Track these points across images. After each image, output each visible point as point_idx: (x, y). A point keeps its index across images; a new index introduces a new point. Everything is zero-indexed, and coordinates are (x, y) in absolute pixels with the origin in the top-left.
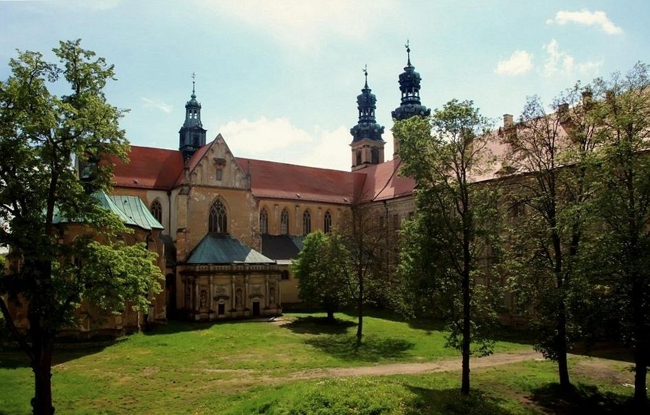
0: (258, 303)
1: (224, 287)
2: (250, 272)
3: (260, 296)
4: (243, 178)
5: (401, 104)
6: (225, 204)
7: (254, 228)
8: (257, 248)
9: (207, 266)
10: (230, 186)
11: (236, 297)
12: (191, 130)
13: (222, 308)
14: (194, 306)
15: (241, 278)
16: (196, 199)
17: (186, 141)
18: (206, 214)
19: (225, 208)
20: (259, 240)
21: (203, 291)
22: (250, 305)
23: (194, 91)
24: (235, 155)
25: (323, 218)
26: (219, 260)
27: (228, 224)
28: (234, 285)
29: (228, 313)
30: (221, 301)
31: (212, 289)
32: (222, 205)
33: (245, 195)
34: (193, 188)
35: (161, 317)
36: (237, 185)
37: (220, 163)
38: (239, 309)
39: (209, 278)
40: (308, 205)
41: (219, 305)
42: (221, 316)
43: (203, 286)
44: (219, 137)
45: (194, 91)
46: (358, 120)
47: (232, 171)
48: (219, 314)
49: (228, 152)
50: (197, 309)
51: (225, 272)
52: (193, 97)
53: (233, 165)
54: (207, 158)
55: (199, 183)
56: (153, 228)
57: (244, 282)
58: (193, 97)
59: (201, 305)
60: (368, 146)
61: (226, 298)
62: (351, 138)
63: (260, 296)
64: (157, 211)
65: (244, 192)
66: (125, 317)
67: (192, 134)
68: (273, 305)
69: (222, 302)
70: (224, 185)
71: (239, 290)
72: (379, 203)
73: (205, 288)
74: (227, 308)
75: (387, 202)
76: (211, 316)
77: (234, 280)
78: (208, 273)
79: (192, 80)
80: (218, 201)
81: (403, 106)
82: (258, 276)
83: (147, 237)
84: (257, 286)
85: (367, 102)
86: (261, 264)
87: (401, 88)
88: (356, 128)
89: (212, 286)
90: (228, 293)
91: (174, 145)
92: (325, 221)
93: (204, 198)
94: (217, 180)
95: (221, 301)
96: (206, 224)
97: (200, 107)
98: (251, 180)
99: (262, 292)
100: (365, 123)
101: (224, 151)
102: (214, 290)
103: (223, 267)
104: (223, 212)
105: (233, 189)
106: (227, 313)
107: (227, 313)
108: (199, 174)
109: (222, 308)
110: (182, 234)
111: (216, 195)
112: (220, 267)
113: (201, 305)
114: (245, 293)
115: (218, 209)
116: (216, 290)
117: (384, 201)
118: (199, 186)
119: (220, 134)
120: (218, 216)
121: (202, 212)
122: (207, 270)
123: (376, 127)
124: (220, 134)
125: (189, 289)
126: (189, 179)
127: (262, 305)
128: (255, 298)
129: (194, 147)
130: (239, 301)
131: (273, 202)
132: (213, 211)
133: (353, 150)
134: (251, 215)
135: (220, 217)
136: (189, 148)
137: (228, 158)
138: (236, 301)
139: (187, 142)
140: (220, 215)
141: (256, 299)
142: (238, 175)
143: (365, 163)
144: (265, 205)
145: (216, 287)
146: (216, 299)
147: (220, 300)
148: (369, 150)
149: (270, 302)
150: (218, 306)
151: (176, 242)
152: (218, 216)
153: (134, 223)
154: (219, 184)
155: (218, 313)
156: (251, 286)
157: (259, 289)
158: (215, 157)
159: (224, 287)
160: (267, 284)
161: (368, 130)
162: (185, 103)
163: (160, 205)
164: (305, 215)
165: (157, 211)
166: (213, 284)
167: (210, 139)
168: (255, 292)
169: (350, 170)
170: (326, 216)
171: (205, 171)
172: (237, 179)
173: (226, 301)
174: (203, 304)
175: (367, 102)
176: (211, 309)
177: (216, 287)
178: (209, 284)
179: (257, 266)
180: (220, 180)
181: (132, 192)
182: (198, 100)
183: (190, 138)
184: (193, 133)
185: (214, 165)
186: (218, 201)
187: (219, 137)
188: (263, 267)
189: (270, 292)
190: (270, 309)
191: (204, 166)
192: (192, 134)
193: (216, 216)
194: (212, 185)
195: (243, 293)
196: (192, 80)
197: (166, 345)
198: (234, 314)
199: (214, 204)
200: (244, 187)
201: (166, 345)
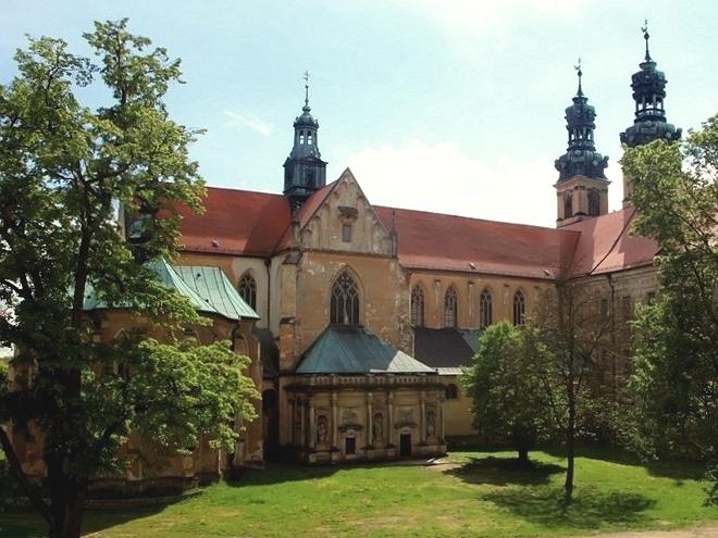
0: (354, 439)
1: (354, 411)
2: (396, 387)
3: (412, 425)
4: (384, 238)
5: (635, 121)
6: (356, 280)
7: (403, 317)
8: (407, 348)
9: (327, 378)
10: (364, 251)
11: (374, 427)
12: (303, 161)
13: (351, 443)
14: (307, 442)
15: (381, 396)
16: (310, 271)
17: (294, 179)
18: (326, 296)
19: (356, 285)
20: (410, 337)
21: (321, 417)
22: (395, 439)
23: (307, 101)
24: (376, 197)
25: (512, 301)
26: (346, 367)
27: (361, 310)
28: (370, 407)
29: (362, 452)
30: (350, 433)
31: (335, 414)
32: (351, 281)
33: (388, 266)
34: (306, 254)
35: (256, 458)
36: (376, 249)
37: (349, 214)
38: (378, 445)
39: (331, 397)
40: (488, 281)
41: (347, 439)
42: (349, 457)
43: (321, 408)
44: (347, 173)
45: (307, 101)
46: (567, 146)
47: (368, 227)
48: (347, 453)
49: (362, 197)
50: (312, 445)
51: (356, 387)
52: (306, 110)
53: (369, 218)
54: (327, 206)
55: (315, 246)
56: (242, 317)
57: (387, 403)
58: (306, 110)
59: (318, 439)
60: (583, 188)
61: (358, 428)
62: (556, 175)
63: (412, 425)
64: (248, 290)
65: (386, 260)
66: (198, 458)
67: (304, 168)
68: (432, 440)
69: (351, 434)
70: (355, 250)
71: (378, 416)
72: (600, 278)
73: (323, 413)
74: (360, 443)
75: (613, 276)
76: (335, 457)
77: (371, 399)
78: (330, 388)
79: (305, 83)
80: (345, 274)
81: (639, 124)
82: (408, 393)
83: (233, 332)
84: (407, 409)
85: (580, 118)
86: (413, 374)
87: (634, 96)
88: (563, 158)
89: (335, 408)
90: (360, 421)
91: (276, 186)
92: (515, 306)
93: (323, 270)
94: (343, 241)
95: (350, 433)
96: (327, 311)
97: (317, 126)
98: (397, 241)
99: (415, 418)
100: (578, 152)
101: (355, 196)
102: (339, 416)
103: (353, 378)
104: (353, 292)
105: (369, 255)
106: (359, 451)
107: (359, 451)
108: (315, 232)
109: (351, 443)
110: (288, 326)
111: (342, 264)
112: (348, 378)
113: (318, 439)
114: (389, 420)
115: (345, 287)
116: (341, 415)
117: (609, 275)
118: (316, 251)
119: (348, 169)
120: (345, 298)
121: (320, 293)
122: (328, 383)
123: (595, 157)
124: (348, 169)
125: (300, 414)
126: (299, 240)
127: (415, 439)
128: (404, 429)
129: (307, 189)
130: (379, 432)
131: (432, 277)
132: (337, 291)
133: (559, 194)
134: (398, 296)
135: (349, 300)
136: (299, 190)
137: (360, 207)
138: (374, 433)
139: (296, 181)
140: (349, 297)
141: (406, 430)
142: (377, 234)
143: (578, 214)
144: (420, 282)
145: (342, 411)
146: (343, 429)
147: (349, 431)
148: (585, 193)
149: (428, 434)
150: (344, 441)
151: (278, 339)
152: (345, 298)
153: (213, 310)
154: (347, 247)
155: (344, 452)
156: (397, 408)
157: (410, 413)
158: (341, 205)
159: (354, 411)
160: (423, 406)
161: (582, 163)
162: (293, 120)
163: (253, 280)
164: (482, 297)
165: (248, 290)
166: (338, 406)
167: (332, 176)
168: (404, 418)
169: (554, 225)
170: (516, 299)
171: (325, 228)
172: (376, 240)
173: (358, 433)
174: (322, 438)
175: (580, 118)
176: (335, 445)
177: (342, 411)
178: (331, 405)
179: (407, 378)
180: (348, 241)
181: (209, 260)
182: (314, 115)
183: (301, 174)
184: (305, 167)
185: (339, 217)
186: (345, 274)
187: (347, 173)
188: (417, 378)
189: (428, 419)
190: (427, 445)
191: (324, 219)
192: (304, 168)
193: (341, 299)
194: (335, 249)
195: (385, 420)
196: (305, 83)
197: (263, 502)
198: (371, 454)
199: (339, 280)
200: (386, 253)
201: (263, 502)
